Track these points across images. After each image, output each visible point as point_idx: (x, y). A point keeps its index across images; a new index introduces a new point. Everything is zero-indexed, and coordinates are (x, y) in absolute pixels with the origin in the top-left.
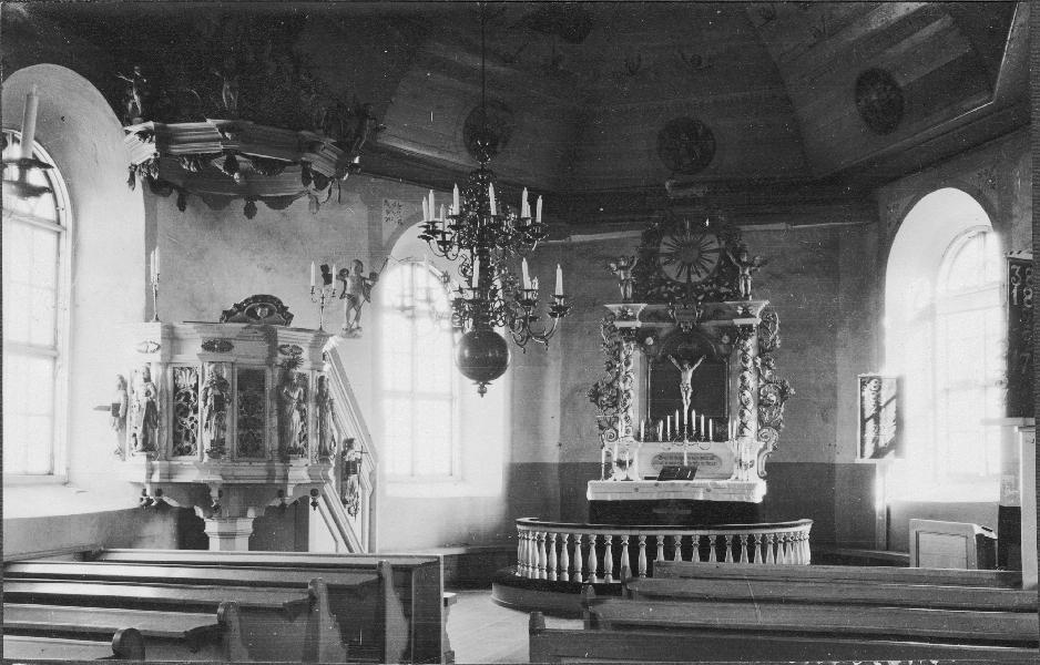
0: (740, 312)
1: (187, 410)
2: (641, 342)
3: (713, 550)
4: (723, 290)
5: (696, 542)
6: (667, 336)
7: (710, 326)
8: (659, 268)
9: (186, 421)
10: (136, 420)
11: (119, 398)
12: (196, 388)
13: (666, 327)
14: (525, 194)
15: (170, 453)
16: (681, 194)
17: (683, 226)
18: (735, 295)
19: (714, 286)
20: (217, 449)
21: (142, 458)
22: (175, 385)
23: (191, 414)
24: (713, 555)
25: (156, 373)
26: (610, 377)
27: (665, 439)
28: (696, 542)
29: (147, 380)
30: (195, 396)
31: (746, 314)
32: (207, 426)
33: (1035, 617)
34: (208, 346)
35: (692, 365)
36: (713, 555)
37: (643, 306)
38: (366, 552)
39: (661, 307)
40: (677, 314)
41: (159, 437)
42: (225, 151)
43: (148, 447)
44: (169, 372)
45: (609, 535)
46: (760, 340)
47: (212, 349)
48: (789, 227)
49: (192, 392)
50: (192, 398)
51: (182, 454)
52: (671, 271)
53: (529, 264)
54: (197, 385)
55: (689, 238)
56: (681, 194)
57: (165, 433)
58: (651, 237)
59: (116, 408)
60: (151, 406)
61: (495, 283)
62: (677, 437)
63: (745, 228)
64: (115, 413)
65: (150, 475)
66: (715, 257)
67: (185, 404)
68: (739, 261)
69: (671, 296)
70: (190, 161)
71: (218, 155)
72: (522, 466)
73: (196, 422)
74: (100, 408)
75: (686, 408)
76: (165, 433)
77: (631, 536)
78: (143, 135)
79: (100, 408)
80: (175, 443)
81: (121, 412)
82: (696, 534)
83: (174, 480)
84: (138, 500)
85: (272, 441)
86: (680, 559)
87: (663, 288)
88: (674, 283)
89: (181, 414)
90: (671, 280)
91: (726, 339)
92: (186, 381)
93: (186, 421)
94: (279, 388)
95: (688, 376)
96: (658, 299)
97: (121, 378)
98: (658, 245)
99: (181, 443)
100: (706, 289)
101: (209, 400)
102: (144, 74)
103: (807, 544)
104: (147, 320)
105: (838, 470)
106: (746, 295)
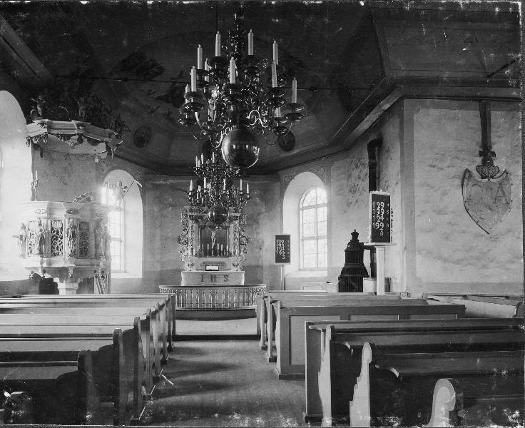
1: (57, 238)
2: (197, 221)
10: (35, 241)
11: (22, 232)
12: (62, 228)
20: (73, 254)
21: (39, 258)
23: (59, 239)
25: (44, 222)
29: (40, 225)
33: (326, 271)
42: (78, 134)
43: (41, 253)
44: (49, 222)
47: (70, 213)
50: (60, 233)
53: (238, 64)
59: (21, 236)
60: (42, 237)
64: (21, 239)
65: (42, 263)
71: (75, 135)
74: (14, 236)
78: (42, 124)
79: (14, 236)
80: (52, 251)
92: (57, 226)
94: (95, 230)
97: (23, 225)
99: (54, 253)
102: (44, 99)
103: (54, 122)
104: (33, 199)
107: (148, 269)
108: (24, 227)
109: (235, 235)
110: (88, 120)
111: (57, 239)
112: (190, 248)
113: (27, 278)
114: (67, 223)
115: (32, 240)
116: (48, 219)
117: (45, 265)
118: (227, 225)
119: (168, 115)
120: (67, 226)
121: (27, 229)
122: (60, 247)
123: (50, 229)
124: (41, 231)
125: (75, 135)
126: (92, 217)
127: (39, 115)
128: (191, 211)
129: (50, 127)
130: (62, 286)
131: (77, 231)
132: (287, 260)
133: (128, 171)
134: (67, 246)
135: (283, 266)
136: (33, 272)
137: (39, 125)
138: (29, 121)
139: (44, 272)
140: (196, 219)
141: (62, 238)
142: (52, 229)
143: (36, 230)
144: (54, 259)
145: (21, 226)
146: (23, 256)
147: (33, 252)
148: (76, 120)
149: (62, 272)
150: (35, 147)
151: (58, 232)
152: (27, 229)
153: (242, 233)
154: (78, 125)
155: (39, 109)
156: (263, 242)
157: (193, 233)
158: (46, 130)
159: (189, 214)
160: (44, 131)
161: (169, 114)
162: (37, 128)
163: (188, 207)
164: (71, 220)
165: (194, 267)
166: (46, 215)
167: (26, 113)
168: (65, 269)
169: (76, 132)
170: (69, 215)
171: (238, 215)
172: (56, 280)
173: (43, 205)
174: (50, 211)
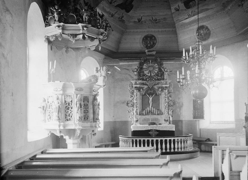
0: (165, 83)
1: (69, 108)
3: (146, 143)
4: (159, 78)
5: (159, 141)
6: (146, 89)
7: (156, 87)
8: (143, 72)
9: (69, 111)
11: (44, 104)
12: (72, 101)
13: (146, 87)
14: (211, 47)
15: (64, 120)
16: (150, 53)
17: (149, 61)
18: (163, 79)
19: (157, 77)
21: (58, 123)
22: (65, 101)
23: (70, 109)
24: (146, 145)
25: (60, 97)
26: (131, 99)
27: (145, 115)
28: (146, 141)
29: (58, 99)
30: (71, 104)
31: (166, 84)
32: (77, 112)
34: (77, 90)
35: (152, 96)
36: (146, 145)
37: (140, 81)
38: (168, 151)
39: (145, 82)
40: (149, 84)
41: (61, 115)
42: (83, 33)
44: (63, 97)
45: (138, 139)
46: (168, 90)
48: (175, 63)
49: (70, 103)
50: (70, 104)
51: (68, 121)
52: (146, 72)
54: (72, 101)
55: (151, 64)
56: (150, 53)
57: (63, 115)
58: (141, 65)
61: (203, 72)
62: (148, 114)
63: (164, 62)
64: (43, 109)
65: (59, 126)
66: (157, 69)
67: (68, 106)
68: (164, 71)
69: (146, 79)
70: (71, 36)
72: (107, 122)
73: (72, 111)
75: (150, 106)
76: (63, 115)
77: (152, 140)
78: (59, 26)
80: (66, 118)
81: (45, 108)
82: (159, 139)
83: (66, 128)
84: (47, 134)
85: (91, 116)
86: (151, 146)
87: (144, 77)
88: (147, 76)
89: (67, 109)
90: (146, 75)
91: (160, 90)
92: (69, 100)
93: (69, 111)
95: (151, 99)
96: (143, 79)
97: (44, 99)
98: (143, 66)
100: (155, 77)
101: (77, 105)
103: (66, 25)
104: (49, 81)
105: (184, 122)
106: (166, 79)
107: (106, 121)
108: (45, 101)
109: (166, 99)
110: (89, 23)
111: (68, 109)
112: (136, 109)
113: (47, 136)
114: (75, 97)
115: (50, 109)
116: (62, 95)
117: (62, 128)
118: (159, 93)
119: (121, 18)
120: (75, 100)
121: (47, 102)
122: (71, 115)
123: (64, 101)
124: (59, 103)
125: (81, 34)
126: (91, 92)
127: (55, 20)
128: (136, 84)
129: (63, 29)
130: (69, 141)
131: (82, 103)
132: (202, 117)
133: (93, 57)
134: (76, 113)
135: (199, 121)
136: (50, 132)
137: (57, 27)
138: (47, 24)
139: (60, 132)
140: (139, 89)
141: (72, 108)
142: (65, 102)
143: (55, 105)
144: (67, 122)
145: (43, 100)
146: (45, 121)
147: (52, 118)
148: (81, 23)
149: (71, 132)
150: (49, 42)
151: (69, 103)
152: (47, 102)
153: (170, 98)
154: (83, 27)
155: (56, 15)
156: (182, 104)
157: (137, 98)
158: (61, 31)
159: (134, 86)
160: (59, 31)
161: (122, 17)
162: (54, 30)
163: (133, 82)
164: (79, 95)
165: (138, 122)
166: (61, 92)
167: (45, 19)
168: (74, 131)
169: (81, 32)
170: (77, 92)
171: (168, 86)
172: (66, 137)
173: (59, 85)
174: (64, 88)
